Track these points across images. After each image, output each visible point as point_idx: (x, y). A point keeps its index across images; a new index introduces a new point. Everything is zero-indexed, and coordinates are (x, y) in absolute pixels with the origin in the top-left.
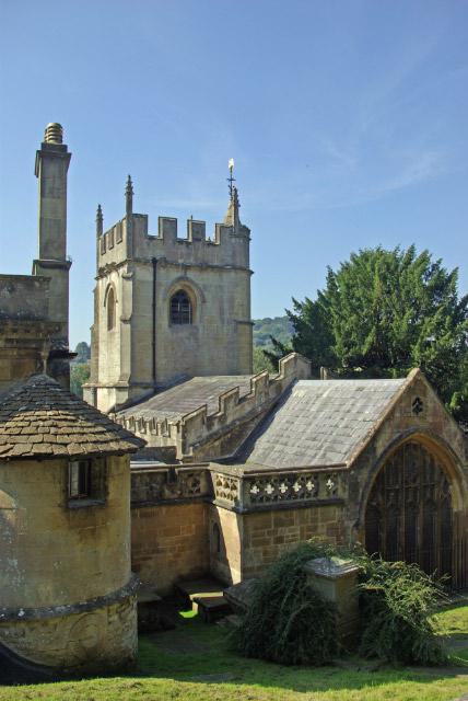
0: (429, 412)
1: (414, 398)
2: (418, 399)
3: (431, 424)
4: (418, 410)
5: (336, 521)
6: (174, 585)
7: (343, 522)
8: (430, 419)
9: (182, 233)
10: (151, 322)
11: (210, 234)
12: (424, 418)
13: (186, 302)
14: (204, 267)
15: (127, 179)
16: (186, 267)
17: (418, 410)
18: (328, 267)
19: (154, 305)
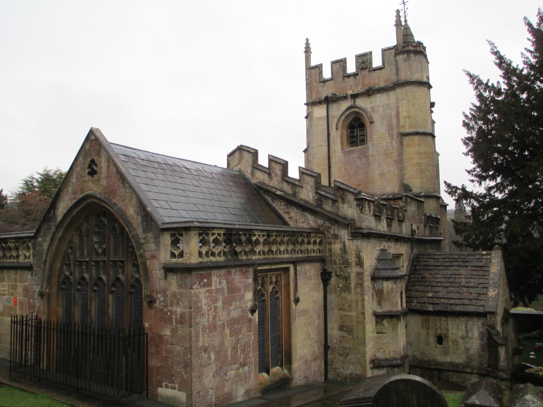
0: (103, 175)
1: (89, 160)
2: (93, 161)
3: (105, 188)
4: (93, 173)
5: (28, 284)
6: (407, 342)
7: (32, 286)
8: (104, 182)
9: (351, 68)
10: (326, 150)
11: (377, 62)
12: (98, 180)
13: (362, 126)
14: (369, 93)
15: (305, 42)
16: (354, 96)
17: (93, 173)
18: (491, 44)
19: (329, 135)
